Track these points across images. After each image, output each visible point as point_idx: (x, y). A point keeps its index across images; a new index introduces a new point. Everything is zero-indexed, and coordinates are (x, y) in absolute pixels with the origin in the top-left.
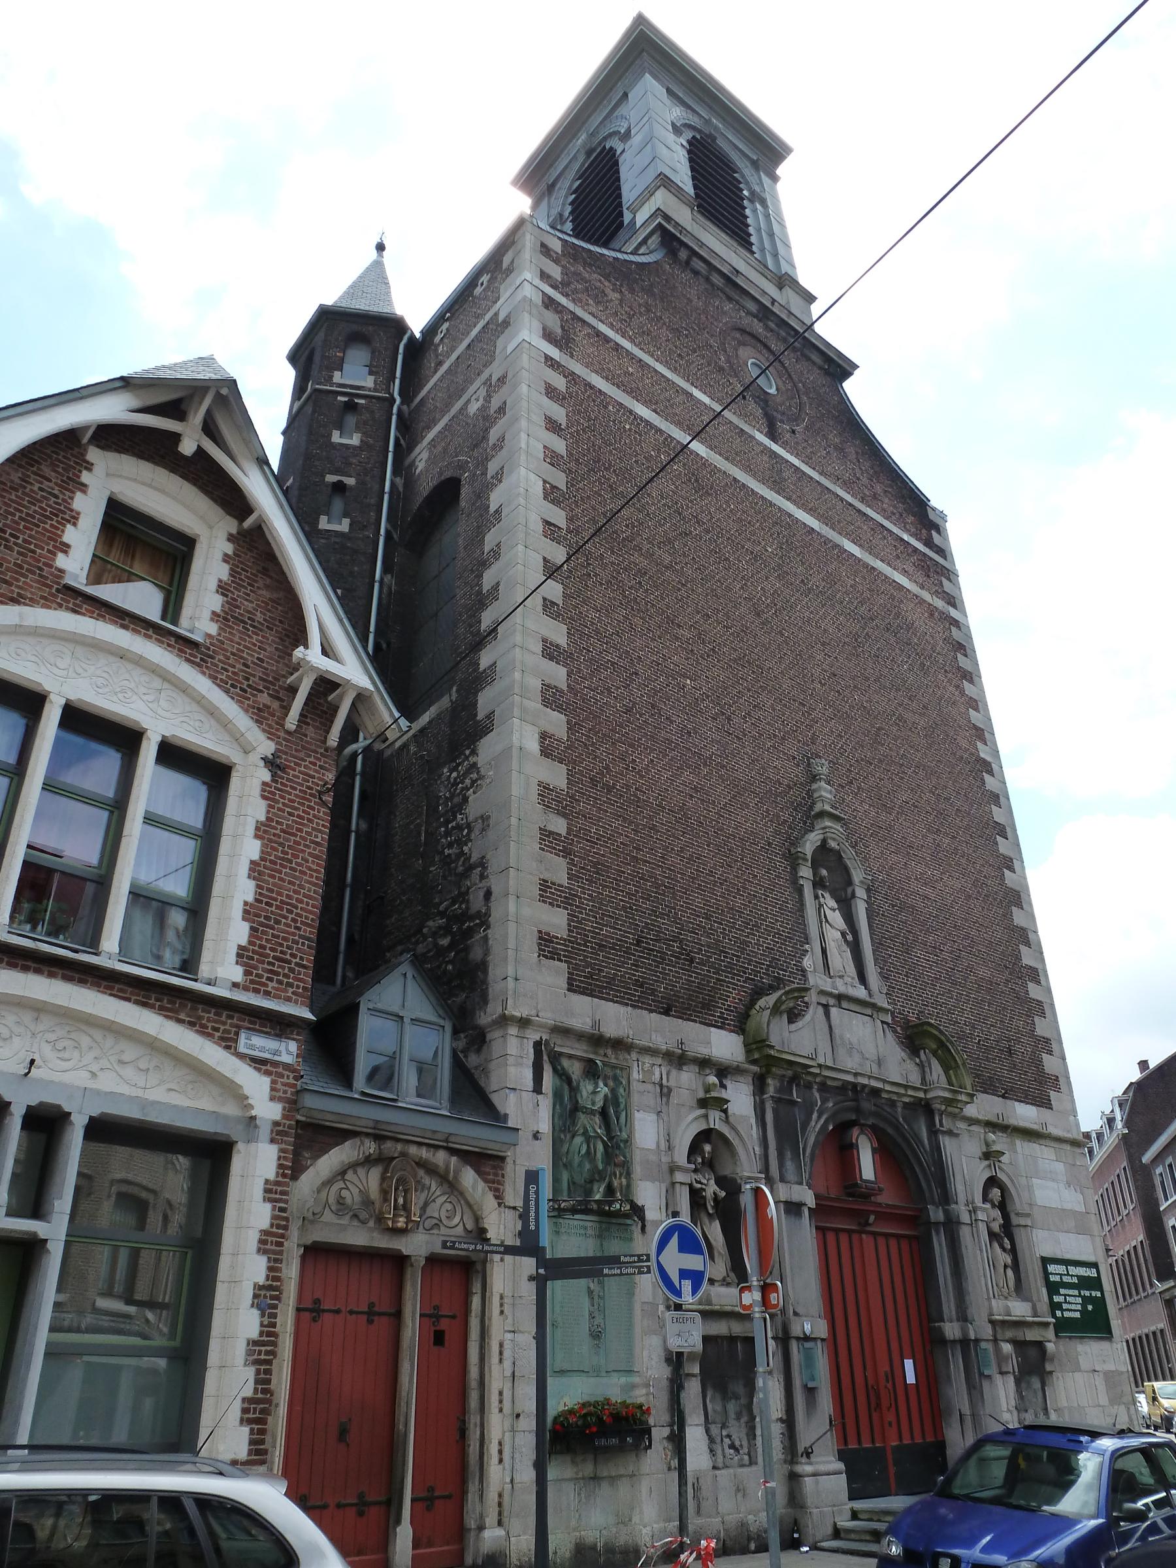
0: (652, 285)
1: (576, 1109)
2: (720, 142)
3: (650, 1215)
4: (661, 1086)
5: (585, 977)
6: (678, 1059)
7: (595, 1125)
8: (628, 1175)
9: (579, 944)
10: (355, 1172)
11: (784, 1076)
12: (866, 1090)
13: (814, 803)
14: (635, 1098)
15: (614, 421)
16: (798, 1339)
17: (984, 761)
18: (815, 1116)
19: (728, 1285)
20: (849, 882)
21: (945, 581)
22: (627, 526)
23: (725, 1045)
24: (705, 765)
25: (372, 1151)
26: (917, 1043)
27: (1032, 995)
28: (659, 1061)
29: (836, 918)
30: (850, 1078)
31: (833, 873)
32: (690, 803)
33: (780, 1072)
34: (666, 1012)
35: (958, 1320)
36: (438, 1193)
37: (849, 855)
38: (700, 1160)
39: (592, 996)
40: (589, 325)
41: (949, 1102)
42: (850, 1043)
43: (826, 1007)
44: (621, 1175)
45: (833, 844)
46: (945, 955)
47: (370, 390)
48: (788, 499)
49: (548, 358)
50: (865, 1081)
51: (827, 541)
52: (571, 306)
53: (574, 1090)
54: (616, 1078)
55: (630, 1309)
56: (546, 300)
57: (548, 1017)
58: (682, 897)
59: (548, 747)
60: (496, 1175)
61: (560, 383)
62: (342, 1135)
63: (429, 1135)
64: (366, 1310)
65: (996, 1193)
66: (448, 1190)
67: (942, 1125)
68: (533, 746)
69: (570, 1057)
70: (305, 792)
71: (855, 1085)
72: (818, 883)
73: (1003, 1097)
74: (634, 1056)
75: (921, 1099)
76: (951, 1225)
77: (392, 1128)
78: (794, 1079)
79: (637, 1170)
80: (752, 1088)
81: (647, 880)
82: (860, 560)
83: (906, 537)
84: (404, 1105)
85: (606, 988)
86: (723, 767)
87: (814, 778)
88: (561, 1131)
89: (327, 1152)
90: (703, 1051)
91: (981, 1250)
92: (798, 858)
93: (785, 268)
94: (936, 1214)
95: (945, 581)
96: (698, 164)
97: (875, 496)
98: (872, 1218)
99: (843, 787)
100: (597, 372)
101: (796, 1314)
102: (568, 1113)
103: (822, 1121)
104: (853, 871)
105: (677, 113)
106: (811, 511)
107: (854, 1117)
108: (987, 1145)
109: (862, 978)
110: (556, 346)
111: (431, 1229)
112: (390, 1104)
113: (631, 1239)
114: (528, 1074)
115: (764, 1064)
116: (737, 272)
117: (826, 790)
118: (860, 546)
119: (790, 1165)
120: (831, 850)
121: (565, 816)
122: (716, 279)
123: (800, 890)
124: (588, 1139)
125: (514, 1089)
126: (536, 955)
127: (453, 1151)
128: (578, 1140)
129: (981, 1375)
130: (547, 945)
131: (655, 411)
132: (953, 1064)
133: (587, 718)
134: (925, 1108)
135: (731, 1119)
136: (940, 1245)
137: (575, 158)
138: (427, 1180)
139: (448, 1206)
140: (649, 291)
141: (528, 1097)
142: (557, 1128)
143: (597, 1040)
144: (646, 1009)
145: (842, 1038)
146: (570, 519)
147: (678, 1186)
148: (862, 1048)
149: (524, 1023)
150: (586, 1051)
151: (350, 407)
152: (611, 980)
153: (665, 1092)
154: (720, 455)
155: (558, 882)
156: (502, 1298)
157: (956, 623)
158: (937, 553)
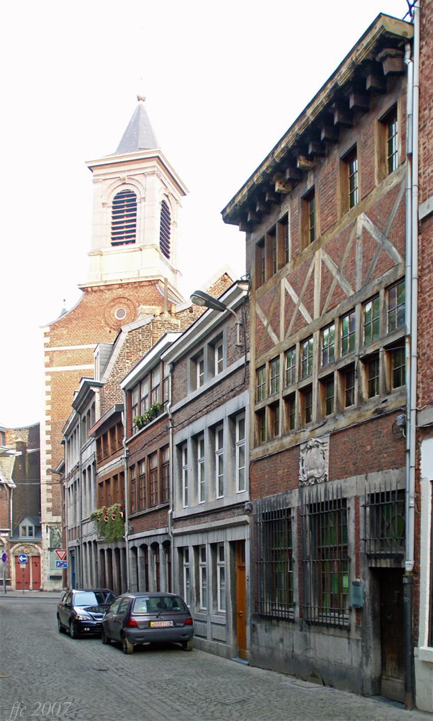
1: (54, 535)
96: (164, 227)
114: (45, 530)
130: (48, 510)
141: (46, 534)
149: (44, 523)
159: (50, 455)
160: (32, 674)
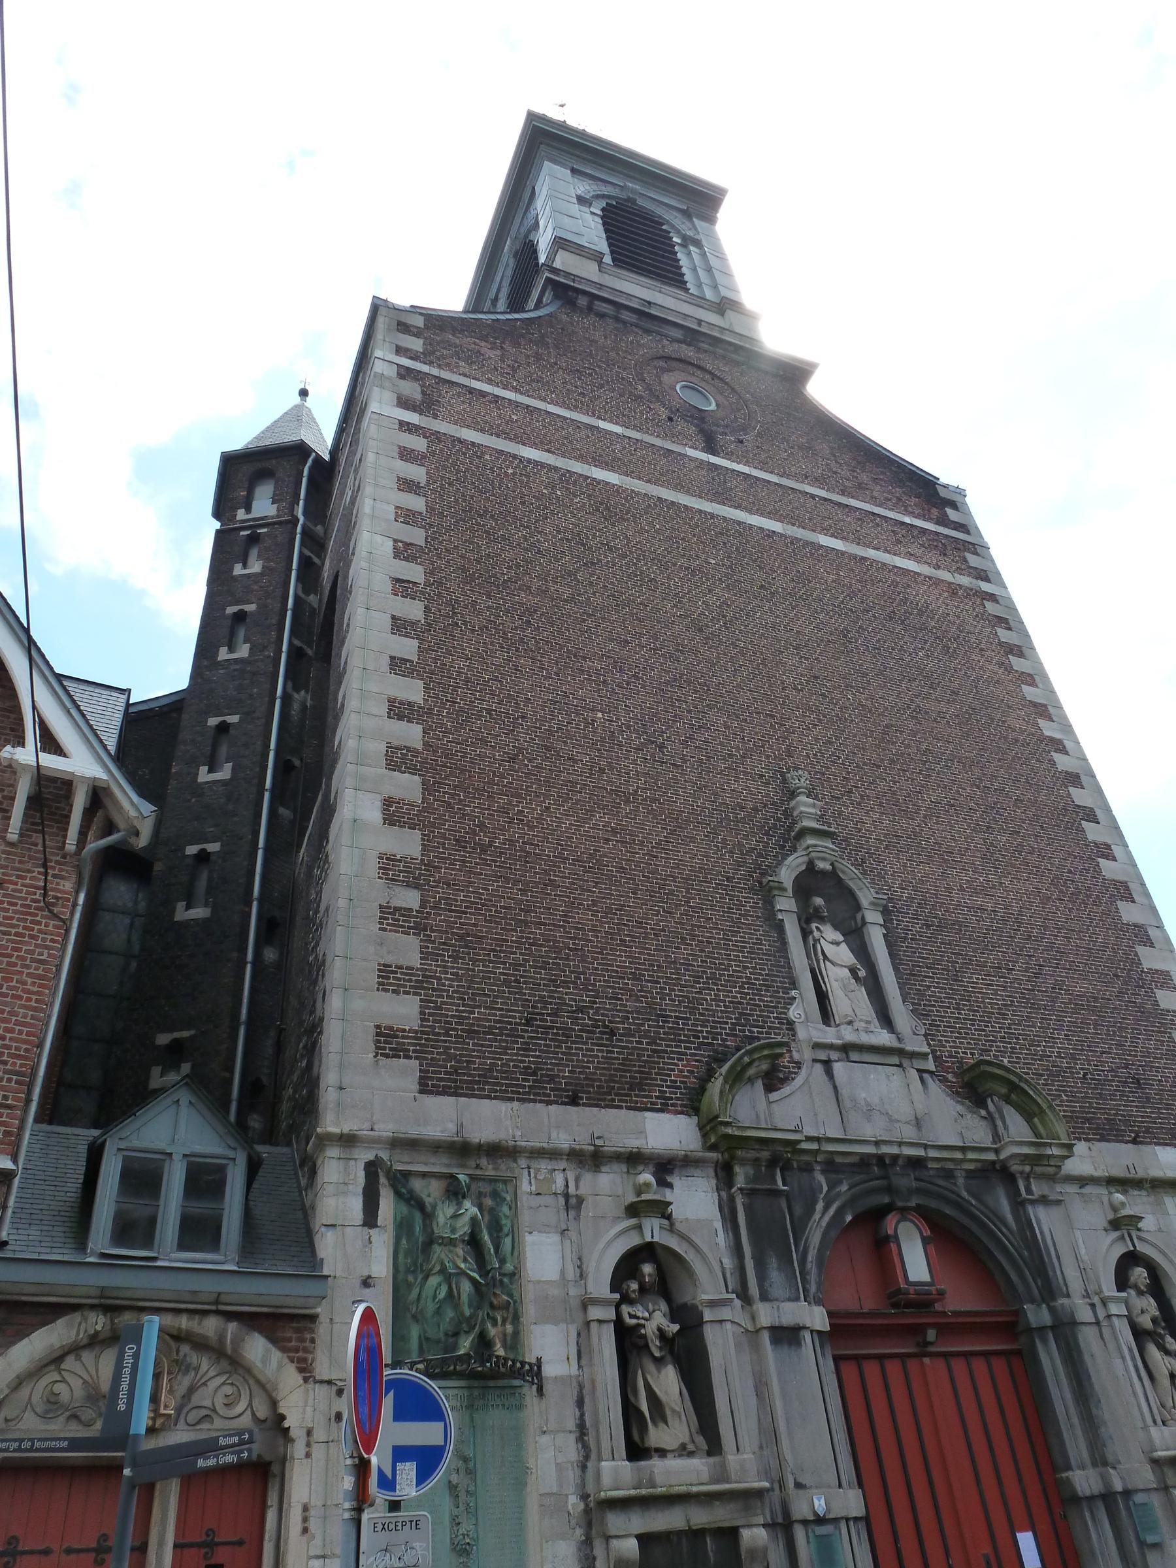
0: (543, 336)
2: (641, 202)
3: (550, 1370)
4: (567, 1196)
5: (446, 1073)
6: (592, 1159)
7: (460, 1259)
8: (516, 1318)
9: (439, 1034)
10: (78, 1358)
11: (757, 1159)
12: (900, 1162)
13: (794, 822)
14: (525, 1217)
15: (492, 469)
16: (805, 1522)
17: (1052, 739)
18: (820, 1206)
19: (691, 1454)
20: (858, 907)
21: (969, 556)
22: (510, 568)
23: (669, 1132)
24: (627, 801)
25: (99, 1328)
26: (980, 1090)
27: (1163, 1005)
28: (563, 1164)
29: (843, 954)
30: (870, 1150)
31: (826, 896)
32: (605, 848)
33: (752, 1154)
34: (574, 1101)
35: (1094, 1464)
36: (212, 1373)
37: (850, 873)
38: (634, 1286)
39: (456, 1094)
40: (459, 385)
41: (1035, 1160)
42: (868, 1104)
43: (827, 1064)
44: (504, 1321)
45: (822, 865)
46: (1019, 975)
47: (273, 517)
48: (736, 508)
49: (402, 424)
50: (894, 1150)
51: (794, 541)
52: (435, 372)
53: (428, 1216)
54: (495, 1195)
55: (521, 1507)
56: (402, 371)
57: (386, 1129)
58: (595, 959)
59: (393, 812)
60: (302, 1340)
61: (419, 444)
62: (51, 1311)
63: (187, 1297)
64: (94, 1545)
65: (1139, 1274)
66: (229, 1368)
67: (1029, 1191)
68: (373, 813)
69: (424, 1175)
70: (29, 907)
71: (880, 1159)
72: (807, 918)
73: (1134, 1142)
74: (523, 1162)
75: (993, 1163)
76: (1065, 1329)
77: (128, 1294)
78: (773, 1162)
79: (530, 1311)
80: (714, 1182)
81: (541, 946)
82: (843, 553)
83: (907, 520)
84: (166, 1264)
85: (478, 1083)
86: (654, 800)
87: (793, 794)
88: (408, 1271)
89: (28, 1335)
90: (633, 1143)
91: (1123, 1358)
92: (771, 889)
93: (724, 292)
94: (1037, 1315)
95: (969, 556)
97: (860, 486)
98: (931, 1335)
99: (838, 799)
100: (468, 427)
101: (799, 1485)
102: (416, 1248)
103: (832, 1211)
104: (859, 894)
105: (583, 187)
106: (770, 515)
107: (887, 1200)
108: (1115, 1209)
109: (886, 1019)
110: (415, 411)
111: (198, 1423)
112: (148, 1266)
113: (520, 1407)
114: (355, 1205)
115: (725, 1151)
116: (649, 303)
117: (806, 805)
118: (843, 538)
119: (776, 1277)
120: (823, 872)
121: (416, 887)
122: (626, 316)
123: (780, 927)
124: (448, 1277)
125: (334, 1226)
126: (371, 1055)
127: (230, 1316)
128: (433, 1281)
129: (1142, 1544)
130: (388, 1043)
131: (548, 451)
132: (1036, 1109)
133: (452, 775)
134: (998, 1173)
135: (679, 1226)
136: (1052, 1359)
137: (507, 265)
138: (194, 1358)
139: (228, 1390)
140: (541, 342)
141: (355, 1234)
142: (402, 1268)
143: (462, 1150)
144: (541, 1101)
145: (853, 1100)
146: (430, 573)
147: (594, 1326)
148: (896, 1108)
149: (348, 1140)
150: (448, 1166)
151: (254, 539)
152: (486, 1074)
153: (573, 1203)
154: (639, 479)
155: (405, 964)
156: (306, 1508)
157: (992, 597)
158: (955, 529)
159: (421, 341)
160: (513, 758)
